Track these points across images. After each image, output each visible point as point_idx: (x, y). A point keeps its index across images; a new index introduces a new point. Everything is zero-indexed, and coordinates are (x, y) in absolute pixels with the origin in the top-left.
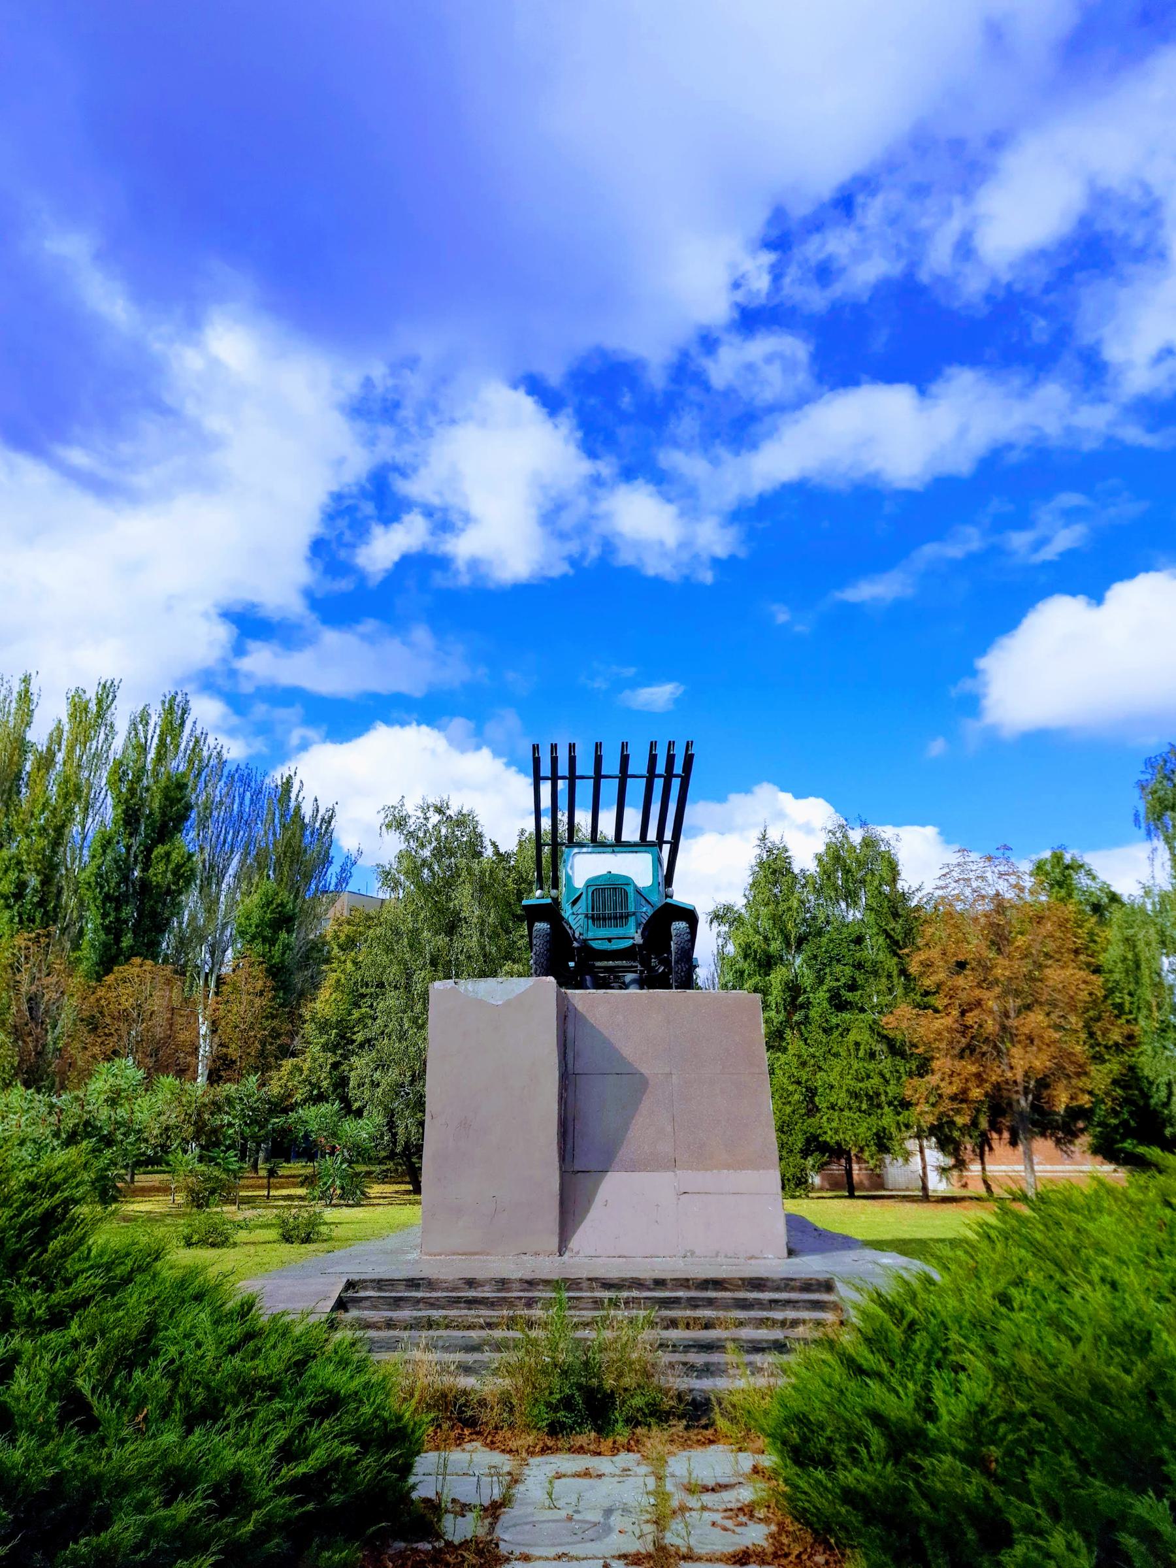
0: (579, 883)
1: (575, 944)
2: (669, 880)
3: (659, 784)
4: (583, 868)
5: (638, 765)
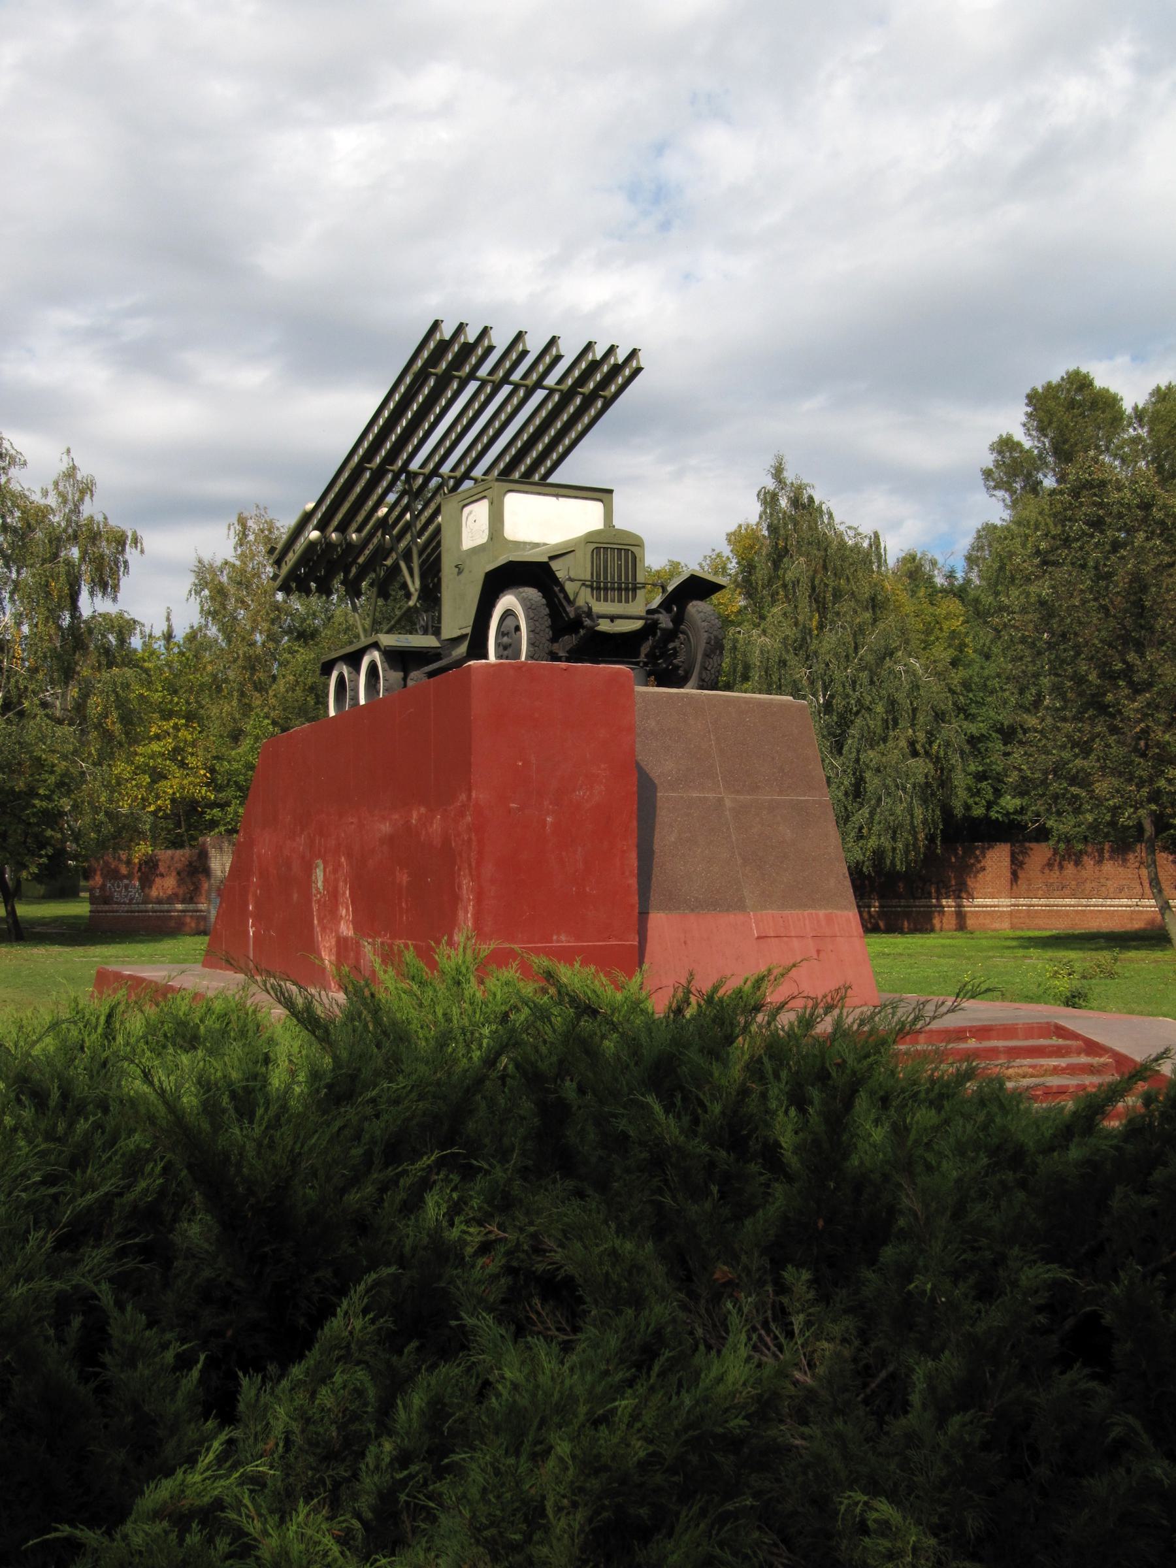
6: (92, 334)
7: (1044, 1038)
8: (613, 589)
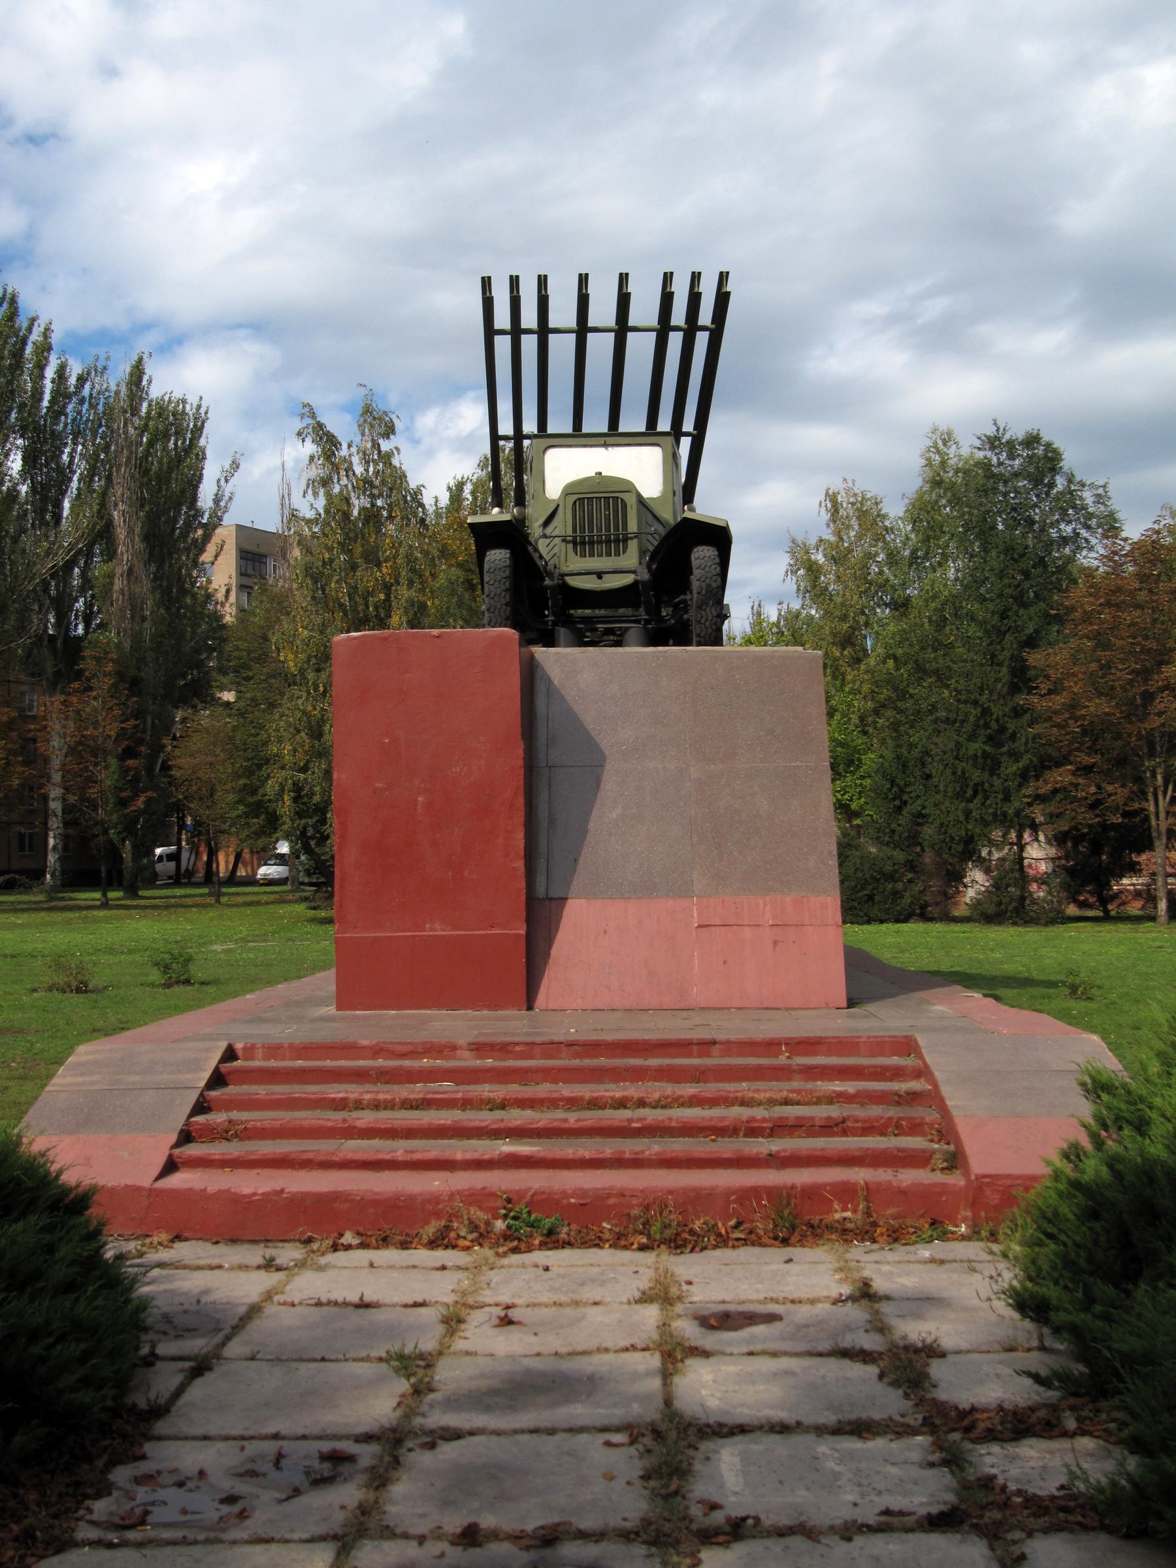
0: (554, 488)
1: (547, 582)
2: (689, 492)
3: (675, 341)
4: (563, 469)
5: (644, 311)
6: (895, 319)
7: (900, 1055)
8: (600, 542)
